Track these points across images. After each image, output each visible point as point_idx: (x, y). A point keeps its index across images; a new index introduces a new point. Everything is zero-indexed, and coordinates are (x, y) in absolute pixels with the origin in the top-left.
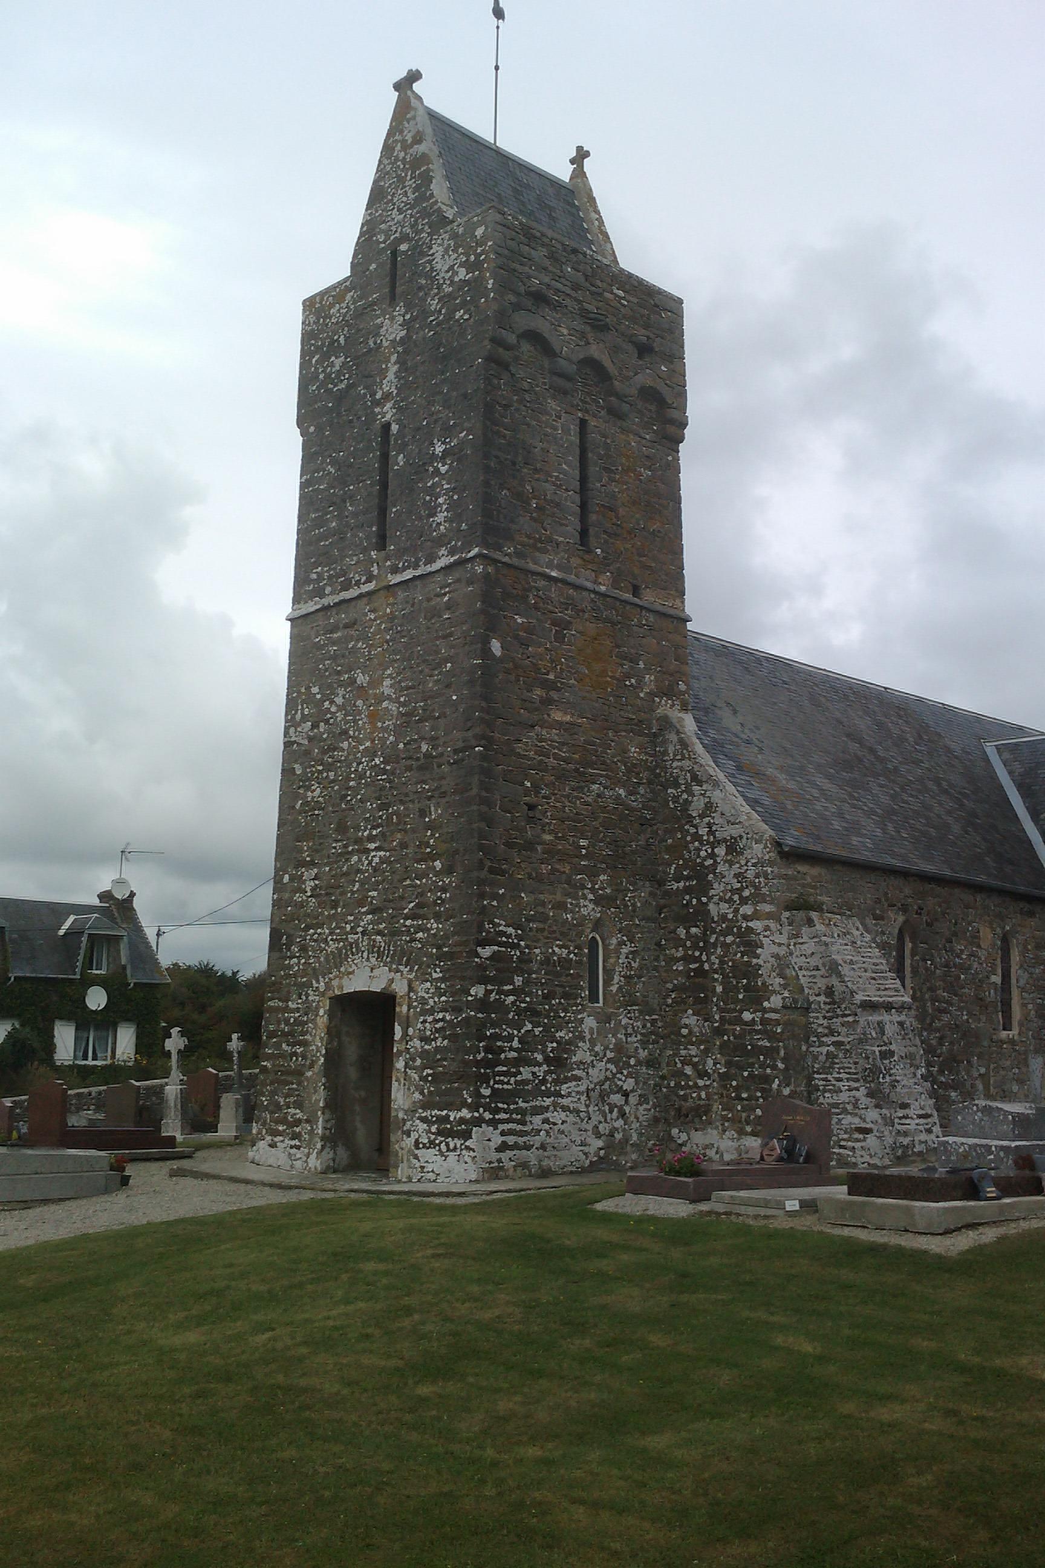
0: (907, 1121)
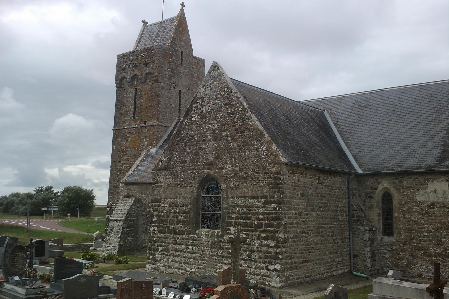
0: (109, 247)
